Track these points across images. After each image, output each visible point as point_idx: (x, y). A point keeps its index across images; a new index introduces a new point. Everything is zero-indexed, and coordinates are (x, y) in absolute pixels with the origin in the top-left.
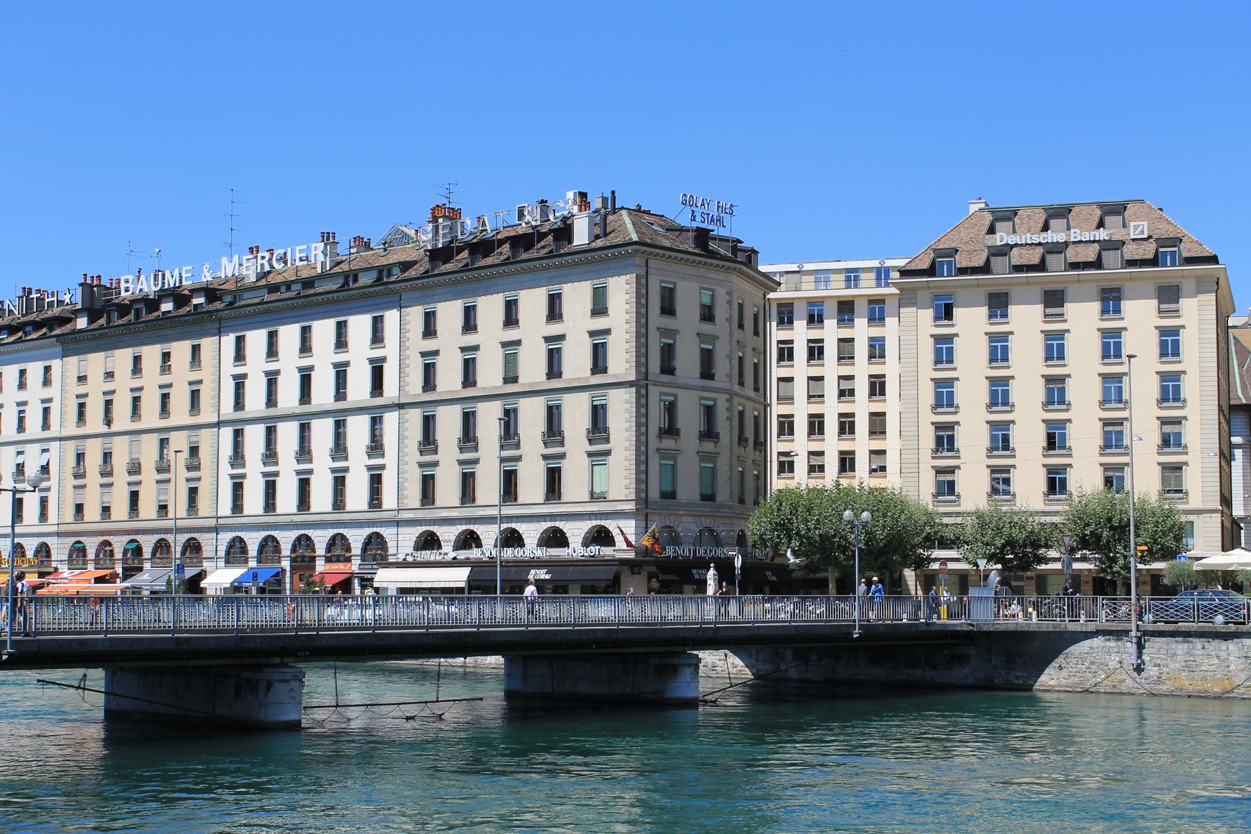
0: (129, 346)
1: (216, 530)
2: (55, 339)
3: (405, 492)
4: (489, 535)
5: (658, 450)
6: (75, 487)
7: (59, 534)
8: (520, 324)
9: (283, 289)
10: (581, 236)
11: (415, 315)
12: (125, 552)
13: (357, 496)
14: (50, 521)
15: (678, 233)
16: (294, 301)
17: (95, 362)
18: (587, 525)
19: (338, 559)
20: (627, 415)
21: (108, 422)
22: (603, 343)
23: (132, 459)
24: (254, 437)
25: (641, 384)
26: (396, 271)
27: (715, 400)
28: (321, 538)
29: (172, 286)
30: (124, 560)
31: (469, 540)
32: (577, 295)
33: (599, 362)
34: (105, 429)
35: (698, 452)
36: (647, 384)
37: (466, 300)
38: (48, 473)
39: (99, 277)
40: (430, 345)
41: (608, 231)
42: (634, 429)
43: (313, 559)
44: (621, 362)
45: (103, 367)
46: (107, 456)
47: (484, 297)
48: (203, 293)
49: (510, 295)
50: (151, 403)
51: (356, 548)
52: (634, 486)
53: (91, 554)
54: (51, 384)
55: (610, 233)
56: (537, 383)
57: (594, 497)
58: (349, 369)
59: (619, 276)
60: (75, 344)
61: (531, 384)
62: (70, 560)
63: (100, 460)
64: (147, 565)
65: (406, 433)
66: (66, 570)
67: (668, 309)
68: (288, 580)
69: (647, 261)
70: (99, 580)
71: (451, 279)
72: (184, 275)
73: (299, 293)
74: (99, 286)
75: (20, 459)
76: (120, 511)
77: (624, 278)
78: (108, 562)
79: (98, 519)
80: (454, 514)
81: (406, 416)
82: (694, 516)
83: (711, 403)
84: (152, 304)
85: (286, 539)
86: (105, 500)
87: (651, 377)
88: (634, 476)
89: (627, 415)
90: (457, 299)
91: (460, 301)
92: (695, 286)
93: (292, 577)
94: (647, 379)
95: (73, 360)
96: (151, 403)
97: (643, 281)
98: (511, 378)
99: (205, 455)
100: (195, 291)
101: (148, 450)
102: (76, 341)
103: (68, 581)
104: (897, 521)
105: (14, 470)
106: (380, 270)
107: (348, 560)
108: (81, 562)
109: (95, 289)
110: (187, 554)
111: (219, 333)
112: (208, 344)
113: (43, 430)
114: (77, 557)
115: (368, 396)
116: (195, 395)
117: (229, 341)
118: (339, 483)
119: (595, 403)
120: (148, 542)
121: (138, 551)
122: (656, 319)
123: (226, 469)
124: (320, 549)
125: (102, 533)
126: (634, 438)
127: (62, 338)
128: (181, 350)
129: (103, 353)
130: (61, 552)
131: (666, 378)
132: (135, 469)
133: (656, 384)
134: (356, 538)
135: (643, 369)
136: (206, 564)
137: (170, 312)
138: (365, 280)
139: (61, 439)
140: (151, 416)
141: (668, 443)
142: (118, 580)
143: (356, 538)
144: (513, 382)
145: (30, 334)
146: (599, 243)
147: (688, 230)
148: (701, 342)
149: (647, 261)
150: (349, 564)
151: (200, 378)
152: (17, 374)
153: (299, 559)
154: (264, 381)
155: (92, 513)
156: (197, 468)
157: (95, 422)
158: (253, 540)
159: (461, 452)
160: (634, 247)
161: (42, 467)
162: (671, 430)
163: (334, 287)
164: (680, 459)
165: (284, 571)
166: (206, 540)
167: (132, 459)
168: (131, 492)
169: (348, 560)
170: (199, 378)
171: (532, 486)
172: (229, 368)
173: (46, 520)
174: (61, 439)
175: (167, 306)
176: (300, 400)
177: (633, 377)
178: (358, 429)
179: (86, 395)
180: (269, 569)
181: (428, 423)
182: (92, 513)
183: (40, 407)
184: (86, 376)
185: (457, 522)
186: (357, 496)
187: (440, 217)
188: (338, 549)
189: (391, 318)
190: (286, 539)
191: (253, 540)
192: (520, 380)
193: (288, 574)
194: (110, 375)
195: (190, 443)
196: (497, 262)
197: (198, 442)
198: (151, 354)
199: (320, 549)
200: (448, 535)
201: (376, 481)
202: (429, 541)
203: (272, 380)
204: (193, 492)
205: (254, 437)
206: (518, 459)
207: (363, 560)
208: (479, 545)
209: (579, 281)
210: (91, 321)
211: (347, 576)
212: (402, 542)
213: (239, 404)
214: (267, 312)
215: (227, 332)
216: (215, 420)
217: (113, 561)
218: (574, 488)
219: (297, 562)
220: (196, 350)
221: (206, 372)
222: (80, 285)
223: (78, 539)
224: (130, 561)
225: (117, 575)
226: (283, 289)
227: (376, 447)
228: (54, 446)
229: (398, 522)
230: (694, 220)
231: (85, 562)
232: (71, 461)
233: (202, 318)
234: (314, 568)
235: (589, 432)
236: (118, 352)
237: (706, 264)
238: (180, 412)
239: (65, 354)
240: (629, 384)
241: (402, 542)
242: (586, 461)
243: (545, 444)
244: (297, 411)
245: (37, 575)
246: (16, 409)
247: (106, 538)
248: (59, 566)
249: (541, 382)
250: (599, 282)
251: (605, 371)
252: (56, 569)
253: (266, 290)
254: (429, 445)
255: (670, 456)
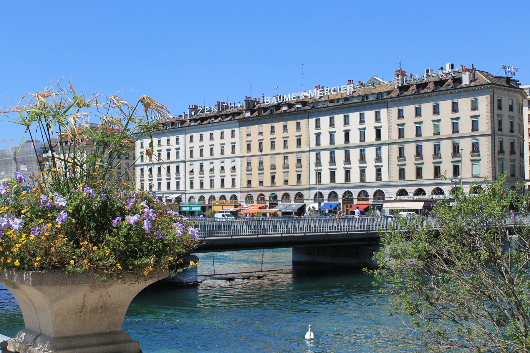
0: (269, 123)
1: (310, 189)
2: (237, 121)
3: (392, 175)
4: (428, 190)
5: (498, 159)
6: (247, 174)
7: (240, 192)
8: (404, 117)
9: (336, 101)
10: (466, 81)
11: (394, 111)
12: (270, 198)
13: (371, 176)
14: (236, 187)
15: (498, 79)
16: (342, 106)
17: (254, 129)
18: (432, 188)
19: (363, 200)
20: (488, 146)
21: (261, 151)
22: (456, 122)
23: (271, 164)
24: (325, 157)
25: (492, 135)
26: (385, 94)
27: (514, 140)
28: (355, 193)
29: (287, 101)
30: (270, 200)
31: (419, 192)
32: (465, 103)
33: (475, 126)
34: (260, 153)
35: (510, 159)
36: (494, 135)
37: (416, 105)
38: (143, 175)
39: (251, 97)
40: (401, 121)
41: (476, 79)
42: (491, 151)
43: (352, 200)
44: (484, 126)
45: (246, 132)
46: (261, 163)
47: (429, 103)
48: (301, 103)
49: (436, 103)
50: (279, 144)
51: (371, 195)
52: (491, 172)
53: (255, 199)
54: (213, 140)
55: (476, 80)
56: (448, 135)
57: (473, 176)
58: (321, 135)
59: (483, 95)
60: (245, 122)
61: (445, 135)
62: (246, 201)
63: (258, 164)
64: (280, 203)
65: (392, 154)
66: (244, 204)
67: (500, 108)
68: (341, 207)
69: (493, 90)
70: (260, 208)
71: (398, 99)
72: (289, 98)
73: (343, 103)
74: (251, 101)
75: (222, 164)
76: (267, 182)
77: (485, 97)
78: (262, 201)
79: (166, 190)
80: (413, 183)
81: (391, 148)
82: (509, 182)
83: (513, 141)
84: (278, 106)
85: (340, 193)
86: (260, 179)
87: (495, 132)
88: (491, 168)
89: (488, 146)
90: (468, 97)
91: (414, 105)
92: (507, 98)
93: (343, 206)
94: (494, 133)
95: (244, 129)
96: (279, 144)
97: (492, 97)
98: (436, 133)
99: (304, 162)
100: (297, 103)
101: (279, 161)
102: (246, 121)
103: (248, 209)
104: (457, 190)
105: (220, 169)
106: (378, 94)
107: (368, 200)
108: (251, 202)
109: (250, 102)
110: (297, 198)
111: (308, 118)
112: (303, 122)
113: (221, 155)
114: (249, 200)
115: (343, 143)
116: (233, 147)
117: (312, 121)
118: (363, 172)
119: (473, 142)
120: (280, 195)
121: (275, 198)
122: (497, 111)
123: (313, 167)
124: (355, 196)
125: (345, 188)
126: (491, 155)
127: (240, 120)
128: (292, 124)
129: (246, 127)
130: (241, 198)
131: (499, 132)
132: (273, 167)
133: (497, 135)
134: (371, 192)
135: (493, 130)
136: (305, 202)
137: (286, 110)
138: (371, 98)
139: (240, 157)
140: (279, 147)
141: (501, 156)
142: (267, 208)
143: (371, 192)
144: (437, 135)
145: (224, 119)
146: (473, 84)
147: (503, 78)
148: (510, 119)
149: (493, 90)
150: (368, 201)
151: (213, 144)
152: (220, 134)
153: (346, 200)
154: (329, 135)
155: (255, 184)
156: (301, 167)
157: (255, 150)
158: (326, 194)
159: (416, 160)
160: (490, 85)
161: (211, 169)
162: (501, 151)
163: (359, 101)
164: (505, 161)
165: (339, 204)
166: (306, 194)
167: (271, 164)
168: (272, 176)
169: (368, 200)
170: (300, 134)
171: (428, 173)
172: (313, 131)
173: (193, 188)
174: (240, 157)
175: (285, 108)
176: (345, 142)
177: (490, 132)
178: (370, 153)
179: (275, 138)
180: (334, 203)
181: (401, 151)
182: (255, 184)
183: (209, 148)
184: (250, 134)
185: (414, 185)
186: (371, 176)
187: (400, 74)
188: (363, 195)
189: (384, 112)
190: (340, 193)
191: (326, 194)
192: (441, 134)
193: (342, 205)
194: (261, 133)
195: (297, 158)
196: (429, 91)
197: (300, 158)
198: (279, 126)
199: (355, 196)
200: (411, 190)
201: (379, 171)
202: (402, 192)
203: (332, 135)
204: (212, 181)
205: (325, 157)
206: (441, 162)
207: (374, 200)
208: (407, 194)
209: (466, 98)
210: (252, 114)
211: (368, 206)
212: (391, 193)
213: (318, 143)
214: (329, 110)
215: (312, 117)
216: (308, 150)
217: (265, 201)
218: (466, 172)
219: (345, 201)
220: (298, 124)
221: (303, 132)
222: (245, 101)
223: (249, 193)
224: (272, 201)
225: (267, 206)
226: (336, 101)
227: (378, 158)
228: (237, 160)
229: (389, 186)
230: (506, 74)
231: (253, 202)
232: (245, 165)
233: (302, 112)
234: (353, 203)
235: (415, 157)
236: (264, 125)
237: (511, 90)
238: (292, 146)
239: (241, 126)
240: (489, 135)
241: (391, 193)
242: (470, 163)
243: (330, 165)
244: (343, 146)
245: (234, 206)
246: (220, 146)
247: (261, 193)
248: (241, 203)
249: (450, 135)
250: (474, 98)
251: (403, 137)
252: (240, 204)
253: (328, 102)
254: (419, 156)
255: (501, 160)
